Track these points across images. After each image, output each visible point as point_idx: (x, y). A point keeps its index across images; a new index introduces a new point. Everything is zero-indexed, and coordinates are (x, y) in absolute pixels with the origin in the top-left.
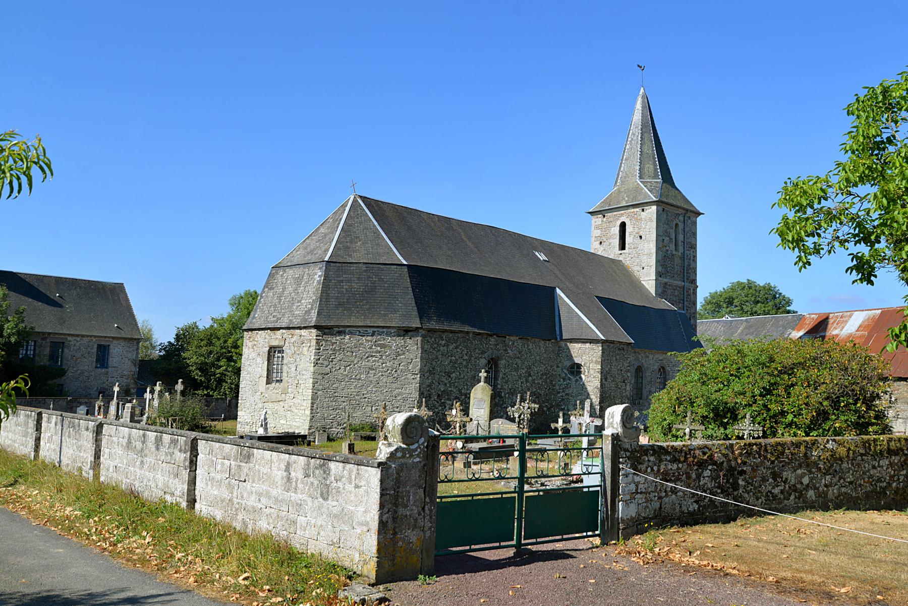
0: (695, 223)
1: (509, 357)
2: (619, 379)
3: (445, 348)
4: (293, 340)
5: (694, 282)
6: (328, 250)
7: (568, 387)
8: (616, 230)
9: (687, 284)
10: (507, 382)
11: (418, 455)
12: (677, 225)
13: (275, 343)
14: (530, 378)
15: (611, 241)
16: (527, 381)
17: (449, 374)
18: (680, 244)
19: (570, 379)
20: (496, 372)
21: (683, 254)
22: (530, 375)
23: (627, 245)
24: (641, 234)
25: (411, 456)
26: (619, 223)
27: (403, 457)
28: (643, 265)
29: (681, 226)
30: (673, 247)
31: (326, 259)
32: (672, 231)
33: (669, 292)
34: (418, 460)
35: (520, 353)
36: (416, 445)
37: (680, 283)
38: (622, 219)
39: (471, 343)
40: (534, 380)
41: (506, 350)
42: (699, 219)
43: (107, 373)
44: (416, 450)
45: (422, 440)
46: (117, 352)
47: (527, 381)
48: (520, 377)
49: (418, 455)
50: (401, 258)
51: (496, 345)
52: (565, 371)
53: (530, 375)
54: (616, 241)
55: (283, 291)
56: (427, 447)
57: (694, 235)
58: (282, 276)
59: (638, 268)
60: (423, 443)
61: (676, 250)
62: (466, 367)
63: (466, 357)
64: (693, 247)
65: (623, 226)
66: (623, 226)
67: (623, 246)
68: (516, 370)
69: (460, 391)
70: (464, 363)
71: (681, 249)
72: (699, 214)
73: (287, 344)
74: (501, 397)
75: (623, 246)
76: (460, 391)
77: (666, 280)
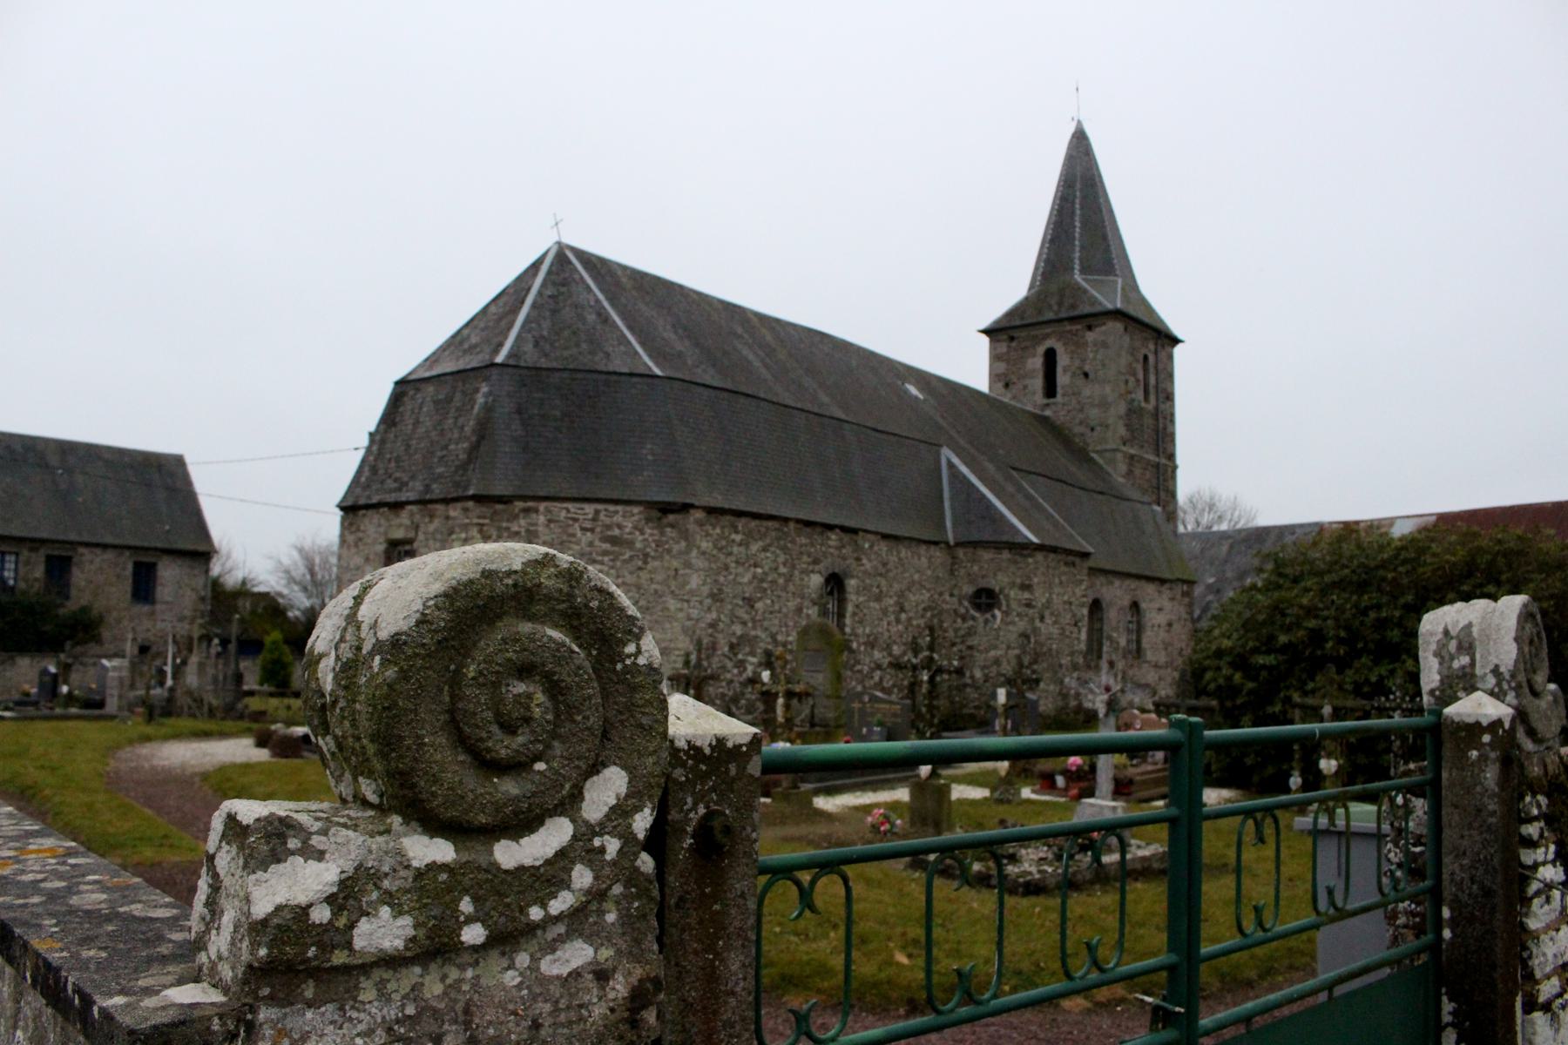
0: (1170, 357)
1: (865, 572)
2: (1067, 618)
3: (742, 549)
4: (431, 528)
5: (1171, 457)
6: (501, 345)
7: (971, 632)
8: (1036, 363)
9: (1163, 461)
10: (861, 622)
11: (578, 921)
12: (1146, 358)
13: (399, 534)
14: (903, 616)
15: (1027, 382)
16: (898, 621)
17: (750, 602)
18: (1152, 390)
19: (974, 618)
20: (842, 602)
21: (1157, 408)
22: (902, 610)
23: (1059, 390)
24: (1087, 368)
25: (504, 940)
26: (1041, 350)
27: (436, 946)
28: (1092, 424)
29: (1151, 359)
30: (1140, 395)
31: (499, 359)
32: (1139, 367)
33: (1138, 472)
34: (578, 954)
35: (885, 565)
36: (554, 836)
37: (1152, 457)
38: (1049, 343)
39: (793, 542)
40: (910, 619)
41: (858, 559)
42: (1178, 351)
43: (153, 613)
44: (550, 876)
45: (607, 789)
46: (169, 574)
47: (898, 621)
48: (885, 612)
49: (578, 921)
50: (651, 364)
51: (839, 548)
52: (966, 603)
53: (902, 610)
54: (1038, 383)
55: (414, 430)
56: (656, 841)
57: (1171, 376)
58: (413, 398)
59: (1081, 429)
60: (621, 812)
61: (1146, 399)
62: (785, 589)
63: (783, 570)
64: (1169, 397)
65: (1050, 356)
66: (1050, 356)
67: (1050, 389)
68: (878, 598)
69: (773, 636)
70: (781, 581)
71: (1152, 398)
72: (1175, 341)
73: (421, 537)
74: (851, 651)
75: (1050, 389)
76: (773, 636)
77: (1132, 451)
